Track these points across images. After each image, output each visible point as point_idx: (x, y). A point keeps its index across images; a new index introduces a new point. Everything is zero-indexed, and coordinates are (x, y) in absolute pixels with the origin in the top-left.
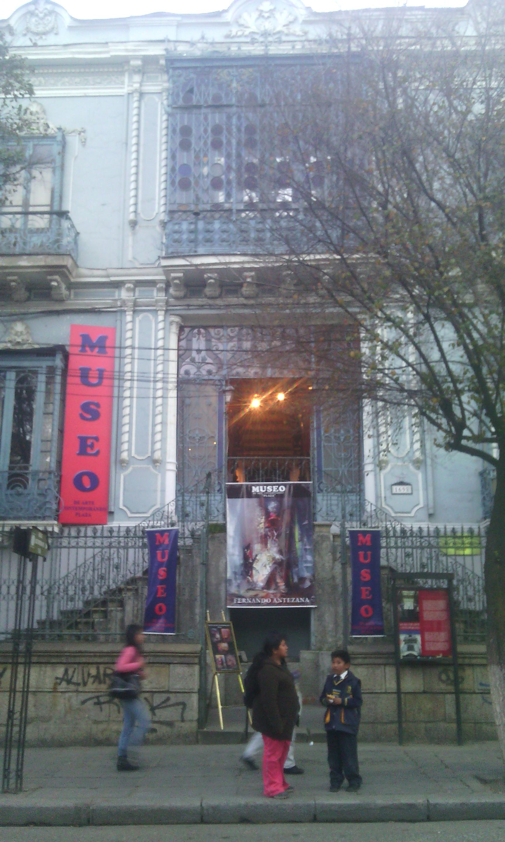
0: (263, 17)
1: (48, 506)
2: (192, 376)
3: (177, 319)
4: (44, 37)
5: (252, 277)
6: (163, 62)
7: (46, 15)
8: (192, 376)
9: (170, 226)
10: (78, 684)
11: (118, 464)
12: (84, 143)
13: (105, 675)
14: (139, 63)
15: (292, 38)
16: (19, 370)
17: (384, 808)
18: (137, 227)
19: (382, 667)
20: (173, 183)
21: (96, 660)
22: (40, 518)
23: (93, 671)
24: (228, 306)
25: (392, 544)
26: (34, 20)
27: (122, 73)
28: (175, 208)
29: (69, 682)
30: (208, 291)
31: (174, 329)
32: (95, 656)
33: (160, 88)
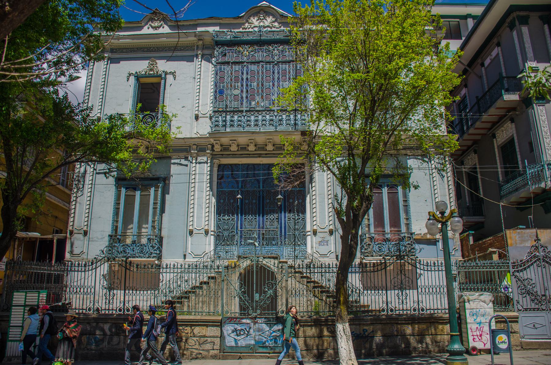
28: (216, 109)
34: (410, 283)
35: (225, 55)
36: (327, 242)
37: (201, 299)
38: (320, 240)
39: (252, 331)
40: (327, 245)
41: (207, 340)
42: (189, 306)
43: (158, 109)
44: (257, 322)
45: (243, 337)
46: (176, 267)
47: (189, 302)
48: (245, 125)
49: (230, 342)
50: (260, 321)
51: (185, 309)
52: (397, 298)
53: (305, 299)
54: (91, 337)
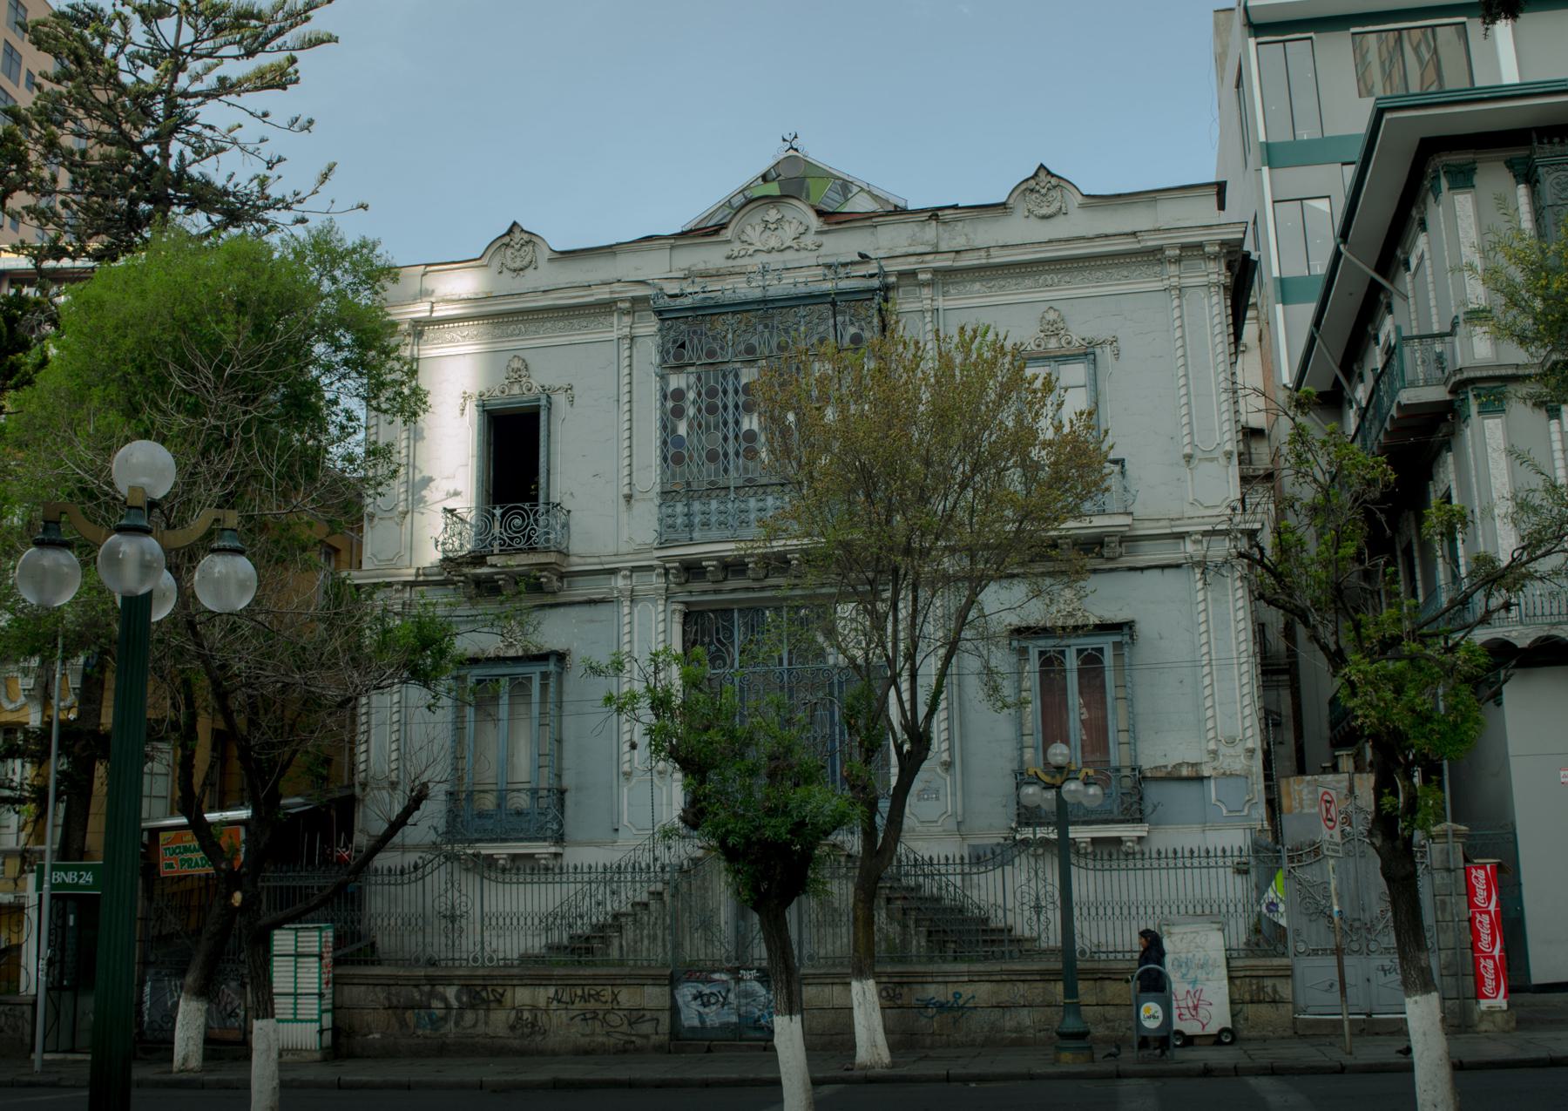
3: (680, 607)
14: (627, 305)
16: (513, 678)
20: (665, 459)
23: (579, 992)
24: (734, 591)
26: (509, 252)
27: (611, 313)
31: (678, 618)
39: (731, 996)
40: (937, 798)
42: (621, 946)
54: (423, 1012)
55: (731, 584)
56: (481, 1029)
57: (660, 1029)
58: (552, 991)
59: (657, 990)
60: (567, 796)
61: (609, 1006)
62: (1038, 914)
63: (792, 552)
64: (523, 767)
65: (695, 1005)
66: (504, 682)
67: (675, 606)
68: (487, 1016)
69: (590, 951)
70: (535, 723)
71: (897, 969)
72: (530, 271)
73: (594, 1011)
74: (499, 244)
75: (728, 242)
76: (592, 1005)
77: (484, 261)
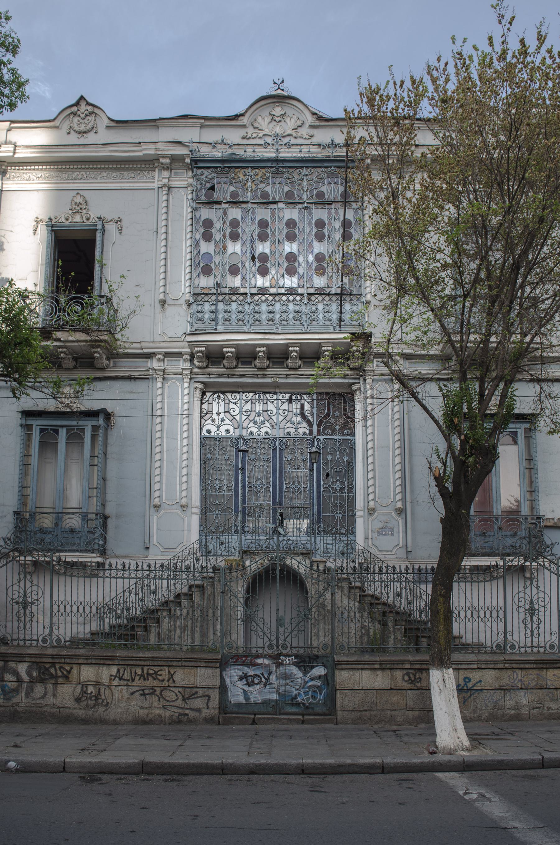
0: (275, 121)
1: (96, 541)
2: (213, 434)
3: (201, 386)
4: (85, 135)
5: (263, 352)
6: (188, 160)
7: (86, 115)
8: (213, 434)
9: (194, 306)
10: (128, 680)
11: (152, 509)
12: (120, 231)
13: (148, 674)
14: (167, 161)
15: (299, 141)
16: (69, 429)
17: (351, 765)
18: (166, 306)
19: (360, 671)
21: (142, 663)
22: (89, 551)
24: (243, 375)
25: (377, 579)
26: (76, 119)
27: (153, 169)
29: (121, 679)
30: (225, 362)
31: (198, 394)
32: (140, 660)
33: (186, 183)
34: (40, 595)
35: (212, 188)
36: (392, 529)
37: (178, 623)
38: (380, 525)
39: (273, 678)
40: (392, 535)
41: (197, 692)
43: (92, 289)
44: (282, 664)
45: (258, 687)
46: (139, 568)
47: (159, 627)
48: (251, 321)
49: (236, 694)
50: (286, 661)
51: (153, 639)
52: (522, 626)
53: (359, 625)
55: (241, 371)
56: (50, 700)
57: (210, 705)
58: (114, 670)
59: (209, 671)
60: (110, 522)
61: (165, 684)
62: (532, 616)
63: (293, 345)
64: (75, 497)
65: (241, 685)
66: (63, 433)
67: (196, 385)
68: (55, 689)
69: (133, 637)
70: (87, 464)
71: (417, 658)
72: (91, 134)
73: (152, 688)
74: (68, 112)
75: (244, 126)
76: (150, 682)
77: (57, 123)
